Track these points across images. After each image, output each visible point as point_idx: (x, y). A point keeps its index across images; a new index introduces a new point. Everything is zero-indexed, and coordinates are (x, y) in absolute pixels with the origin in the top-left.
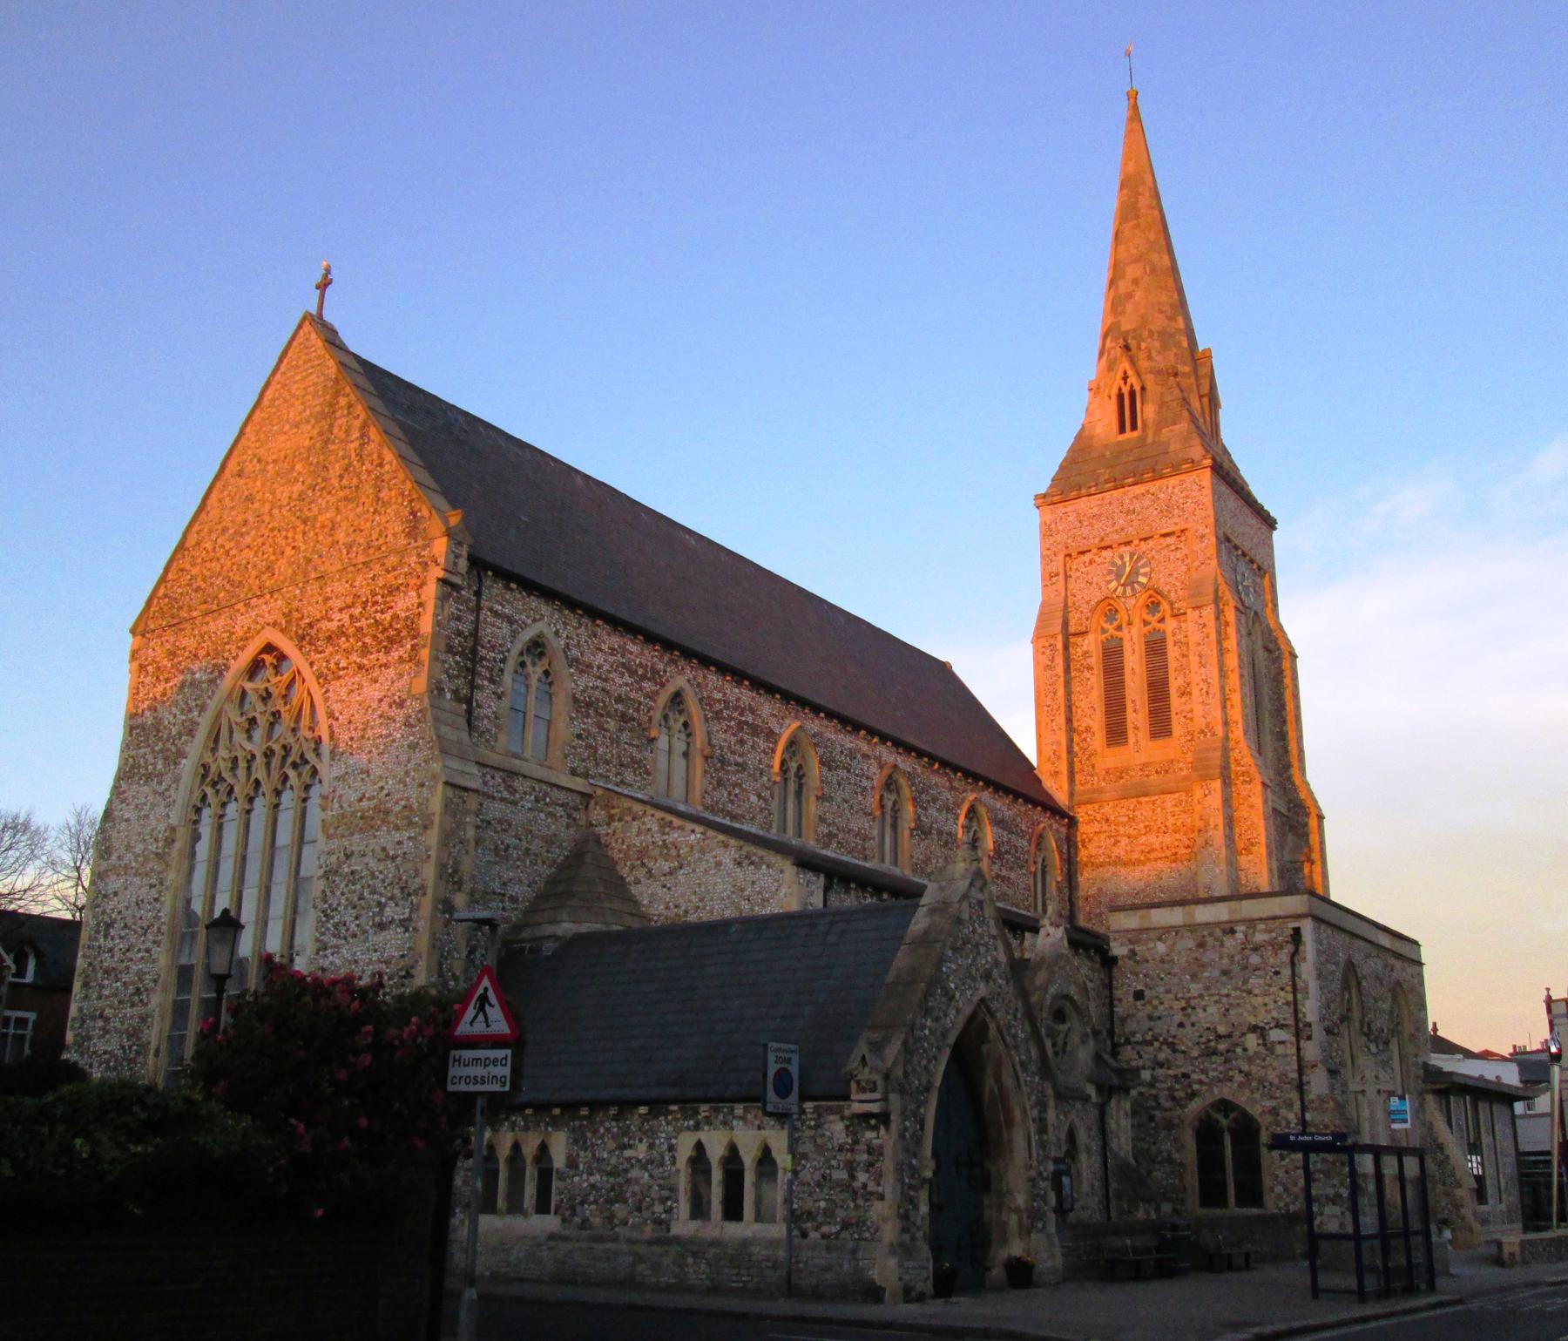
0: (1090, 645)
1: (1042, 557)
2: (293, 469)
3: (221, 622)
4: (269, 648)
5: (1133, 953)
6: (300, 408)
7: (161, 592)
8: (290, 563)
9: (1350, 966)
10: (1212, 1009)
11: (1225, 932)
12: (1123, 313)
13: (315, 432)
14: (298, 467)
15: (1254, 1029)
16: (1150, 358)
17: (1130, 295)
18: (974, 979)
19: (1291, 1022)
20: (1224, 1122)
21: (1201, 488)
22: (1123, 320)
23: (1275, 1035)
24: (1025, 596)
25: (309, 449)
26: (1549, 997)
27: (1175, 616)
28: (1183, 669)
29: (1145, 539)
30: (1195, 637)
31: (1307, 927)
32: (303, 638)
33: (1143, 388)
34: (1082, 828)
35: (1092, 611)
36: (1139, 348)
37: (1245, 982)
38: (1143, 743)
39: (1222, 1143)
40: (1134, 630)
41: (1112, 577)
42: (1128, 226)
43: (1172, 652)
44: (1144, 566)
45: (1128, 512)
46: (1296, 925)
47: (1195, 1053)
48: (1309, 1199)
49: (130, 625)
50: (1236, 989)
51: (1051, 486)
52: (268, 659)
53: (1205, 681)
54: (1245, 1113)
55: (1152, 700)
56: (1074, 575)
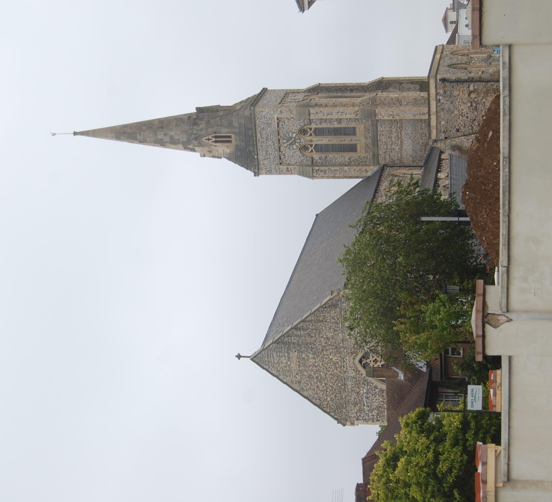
0: (316, 156)
1: (279, 174)
2: (304, 358)
3: (349, 383)
4: (360, 361)
5: (444, 132)
6: (284, 358)
7: (333, 414)
8: (335, 355)
9: (449, 66)
10: (463, 107)
11: (440, 102)
12: (179, 140)
13: (294, 350)
14: (303, 356)
15: (469, 95)
16: (201, 130)
17: (171, 137)
19: (468, 84)
21: (262, 111)
23: (471, 88)
24: (294, 183)
25: (299, 352)
27: (310, 124)
28: (331, 121)
29: (279, 134)
30: (320, 116)
31: (439, 77)
32: (360, 346)
33: (215, 133)
34: (387, 161)
35: (303, 155)
36: (195, 134)
37: (455, 97)
38: (357, 138)
40: (314, 139)
42: (138, 137)
43: (324, 125)
44: (289, 135)
45: (267, 140)
46: (438, 80)
47: (476, 113)
49: (342, 426)
50: (457, 100)
51: (251, 170)
52: (364, 361)
55: (341, 134)
56: (288, 162)
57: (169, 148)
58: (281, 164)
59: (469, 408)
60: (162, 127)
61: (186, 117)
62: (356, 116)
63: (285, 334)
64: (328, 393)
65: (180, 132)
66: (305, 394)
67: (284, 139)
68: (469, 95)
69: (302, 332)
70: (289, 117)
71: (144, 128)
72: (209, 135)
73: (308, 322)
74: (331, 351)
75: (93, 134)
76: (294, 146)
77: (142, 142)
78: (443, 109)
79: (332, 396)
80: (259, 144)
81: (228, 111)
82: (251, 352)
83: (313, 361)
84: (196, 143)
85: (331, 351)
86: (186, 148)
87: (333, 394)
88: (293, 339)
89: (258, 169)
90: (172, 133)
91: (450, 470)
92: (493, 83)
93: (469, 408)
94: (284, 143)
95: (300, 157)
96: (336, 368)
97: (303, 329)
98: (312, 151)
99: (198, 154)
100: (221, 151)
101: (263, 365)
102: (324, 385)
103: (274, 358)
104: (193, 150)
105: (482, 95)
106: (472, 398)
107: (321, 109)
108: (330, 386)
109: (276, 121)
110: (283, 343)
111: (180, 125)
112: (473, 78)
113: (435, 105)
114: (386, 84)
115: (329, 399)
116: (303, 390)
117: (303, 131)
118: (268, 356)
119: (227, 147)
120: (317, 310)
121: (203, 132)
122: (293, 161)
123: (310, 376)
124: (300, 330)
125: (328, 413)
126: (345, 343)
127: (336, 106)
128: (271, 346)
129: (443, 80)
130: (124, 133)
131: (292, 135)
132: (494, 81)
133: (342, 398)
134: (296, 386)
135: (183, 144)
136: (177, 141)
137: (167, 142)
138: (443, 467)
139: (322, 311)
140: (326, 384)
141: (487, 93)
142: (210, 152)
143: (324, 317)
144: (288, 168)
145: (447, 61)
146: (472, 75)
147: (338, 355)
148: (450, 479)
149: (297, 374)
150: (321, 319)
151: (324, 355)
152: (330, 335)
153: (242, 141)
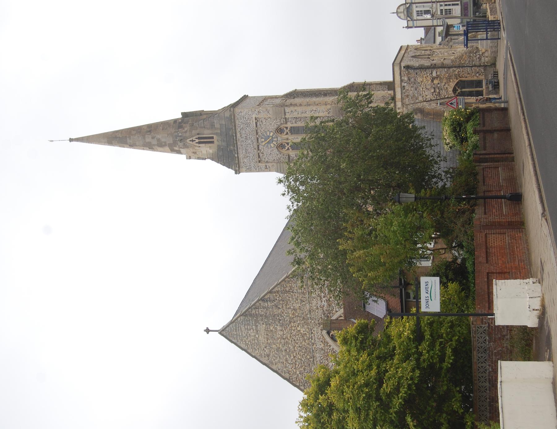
1: (259, 171)
2: (272, 331)
3: (318, 355)
7: (302, 388)
9: (413, 57)
10: (426, 93)
11: (404, 89)
12: (165, 142)
13: (261, 322)
14: (271, 328)
15: (432, 81)
16: (186, 132)
17: (158, 140)
18: (391, 258)
20: (459, 91)
21: (241, 112)
22: (168, 142)
23: (434, 74)
25: (266, 325)
26: (406, 27)
29: (257, 133)
30: (295, 115)
31: (403, 64)
33: (198, 134)
36: (180, 136)
39: (465, 91)
40: (290, 138)
41: (269, 146)
44: (267, 134)
45: (246, 139)
48: (480, 66)
51: (232, 169)
53: (311, 112)
54: (456, 85)
56: (267, 160)
57: (157, 151)
58: (259, 161)
59: (423, 309)
60: (150, 131)
61: (172, 122)
62: (329, 113)
63: (253, 306)
64: (297, 366)
65: (166, 135)
66: (274, 367)
67: (262, 138)
68: (432, 81)
69: (269, 303)
70: (267, 117)
71: (134, 132)
72: (192, 136)
73: (275, 292)
74: (299, 322)
75: (87, 139)
76: (272, 145)
77: (132, 146)
78: (408, 96)
79: (301, 369)
80: (239, 144)
81: (211, 114)
82: (219, 328)
83: (281, 333)
84: (181, 144)
85: (299, 322)
86: (172, 151)
87: (301, 366)
88: (261, 312)
89: (239, 167)
90: (159, 136)
91: (397, 389)
92: (455, 69)
93: (423, 309)
94: (262, 142)
95: (277, 155)
96: (305, 340)
97: (270, 301)
98: (288, 149)
99: (184, 156)
100: (204, 152)
101: (231, 339)
102: (292, 357)
103: (242, 331)
104: (179, 152)
105: (445, 81)
106: (427, 295)
107: (296, 108)
108: (298, 359)
109: (254, 121)
110: (251, 315)
111: (167, 129)
112: (435, 65)
113: (400, 92)
114: (357, 87)
115: (298, 373)
116: (272, 363)
117: (280, 130)
118: (236, 330)
119: (210, 147)
120: (284, 280)
121: (188, 134)
122: (271, 159)
123: (278, 349)
124: (267, 301)
125: (298, 387)
126: (312, 314)
127: (310, 105)
128: (239, 319)
129: (407, 67)
130: (116, 137)
131: (270, 134)
132: (455, 67)
133: (311, 371)
134: (265, 360)
135: (169, 147)
136: (163, 144)
137: (154, 145)
138: (387, 388)
139: (289, 282)
140: (294, 357)
141: (449, 78)
142: (195, 153)
143: (291, 287)
144: (266, 166)
145: (412, 54)
146: (435, 62)
147: (306, 326)
148: (397, 402)
149: (266, 347)
150: (287, 289)
151: (292, 327)
152: (297, 306)
153: (224, 141)
